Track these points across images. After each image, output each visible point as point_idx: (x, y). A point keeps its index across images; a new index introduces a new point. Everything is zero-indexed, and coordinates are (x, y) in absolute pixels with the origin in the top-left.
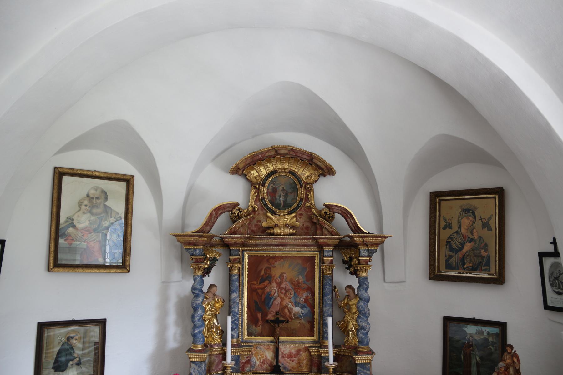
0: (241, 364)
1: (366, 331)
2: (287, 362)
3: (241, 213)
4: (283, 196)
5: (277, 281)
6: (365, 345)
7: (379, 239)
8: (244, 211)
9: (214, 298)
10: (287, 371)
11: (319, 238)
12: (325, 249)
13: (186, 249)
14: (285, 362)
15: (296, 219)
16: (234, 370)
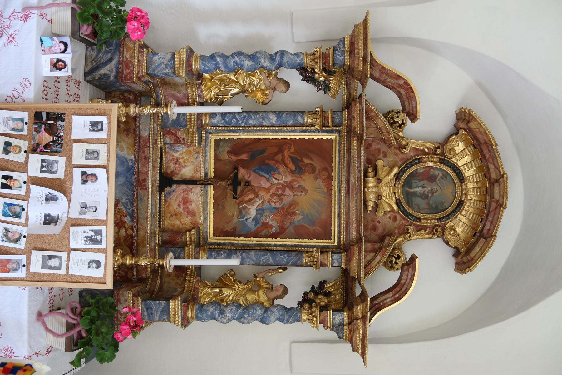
0: (174, 131)
1: (217, 316)
2: (177, 197)
3: (398, 127)
4: (424, 191)
5: (295, 183)
6: (196, 315)
7: (360, 344)
8: (401, 131)
9: (269, 87)
10: (165, 197)
11: (361, 247)
12: (343, 256)
13: (344, 38)
14: (178, 194)
15: (389, 212)
16: (166, 121)
